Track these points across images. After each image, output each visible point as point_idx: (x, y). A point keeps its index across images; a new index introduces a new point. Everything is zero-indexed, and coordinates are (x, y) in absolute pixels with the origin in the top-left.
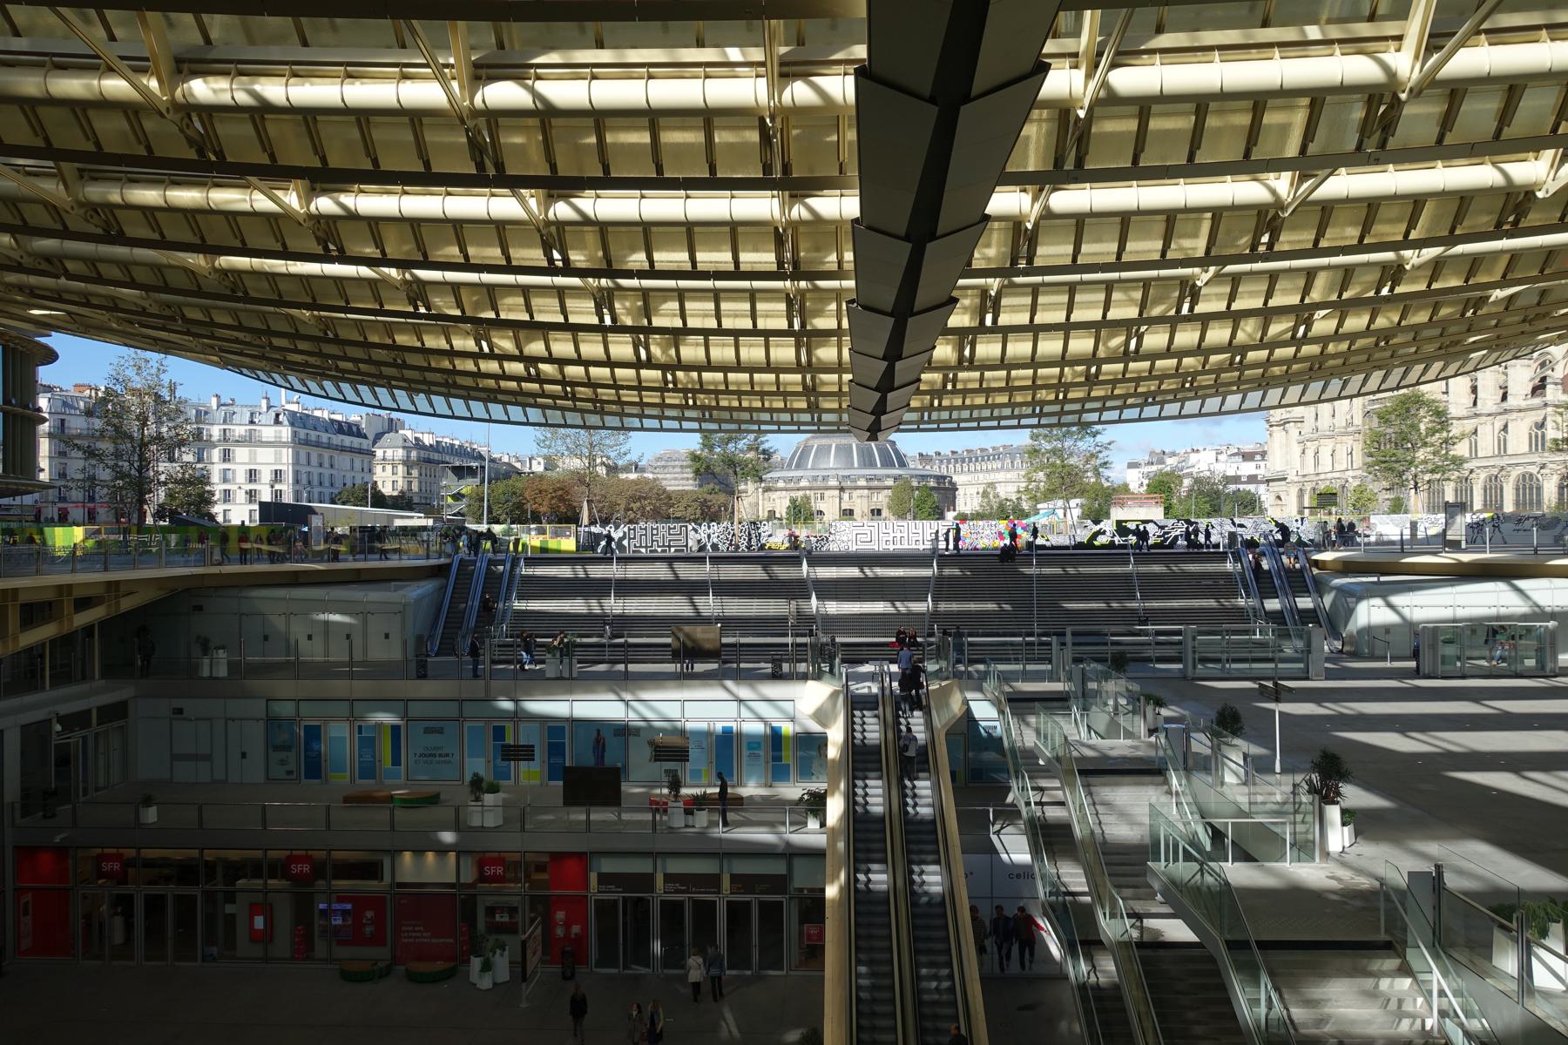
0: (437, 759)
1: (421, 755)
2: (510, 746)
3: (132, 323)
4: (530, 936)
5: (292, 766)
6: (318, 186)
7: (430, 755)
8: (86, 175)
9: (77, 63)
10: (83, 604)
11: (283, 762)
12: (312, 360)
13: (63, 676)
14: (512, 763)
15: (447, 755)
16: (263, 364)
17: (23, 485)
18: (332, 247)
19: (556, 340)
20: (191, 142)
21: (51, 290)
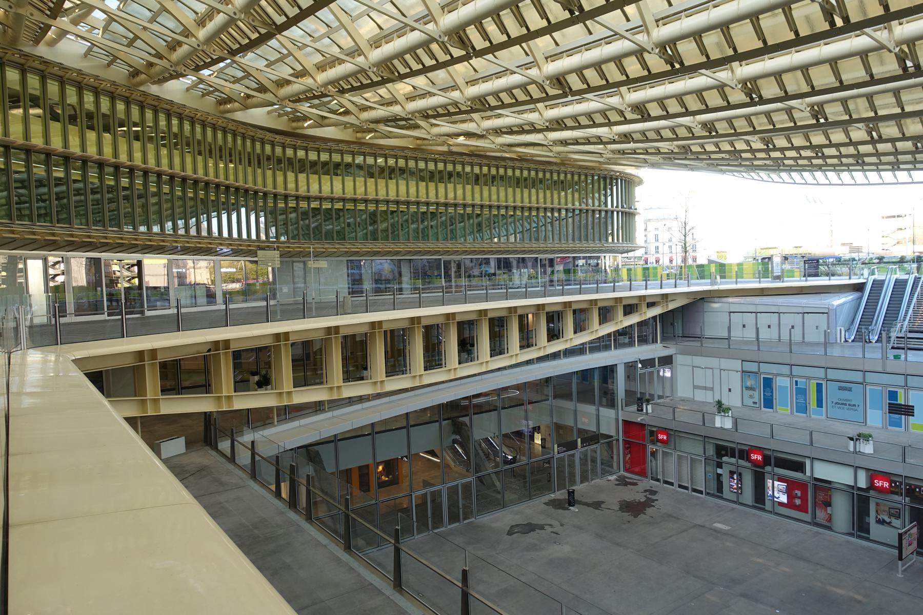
0: (848, 407)
1: (836, 403)
2: (901, 405)
3: (671, 159)
4: (906, 532)
5: (756, 400)
6: (744, 63)
7: (843, 404)
8: (548, 107)
9: (705, 7)
10: (651, 305)
11: (751, 397)
12: (768, 162)
13: (643, 340)
14: (903, 416)
15: (854, 405)
16: (742, 169)
17: (630, 247)
18: (754, 96)
19: (832, 133)
20: (667, 62)
21: (631, 150)
